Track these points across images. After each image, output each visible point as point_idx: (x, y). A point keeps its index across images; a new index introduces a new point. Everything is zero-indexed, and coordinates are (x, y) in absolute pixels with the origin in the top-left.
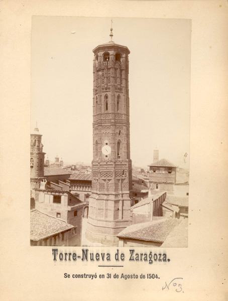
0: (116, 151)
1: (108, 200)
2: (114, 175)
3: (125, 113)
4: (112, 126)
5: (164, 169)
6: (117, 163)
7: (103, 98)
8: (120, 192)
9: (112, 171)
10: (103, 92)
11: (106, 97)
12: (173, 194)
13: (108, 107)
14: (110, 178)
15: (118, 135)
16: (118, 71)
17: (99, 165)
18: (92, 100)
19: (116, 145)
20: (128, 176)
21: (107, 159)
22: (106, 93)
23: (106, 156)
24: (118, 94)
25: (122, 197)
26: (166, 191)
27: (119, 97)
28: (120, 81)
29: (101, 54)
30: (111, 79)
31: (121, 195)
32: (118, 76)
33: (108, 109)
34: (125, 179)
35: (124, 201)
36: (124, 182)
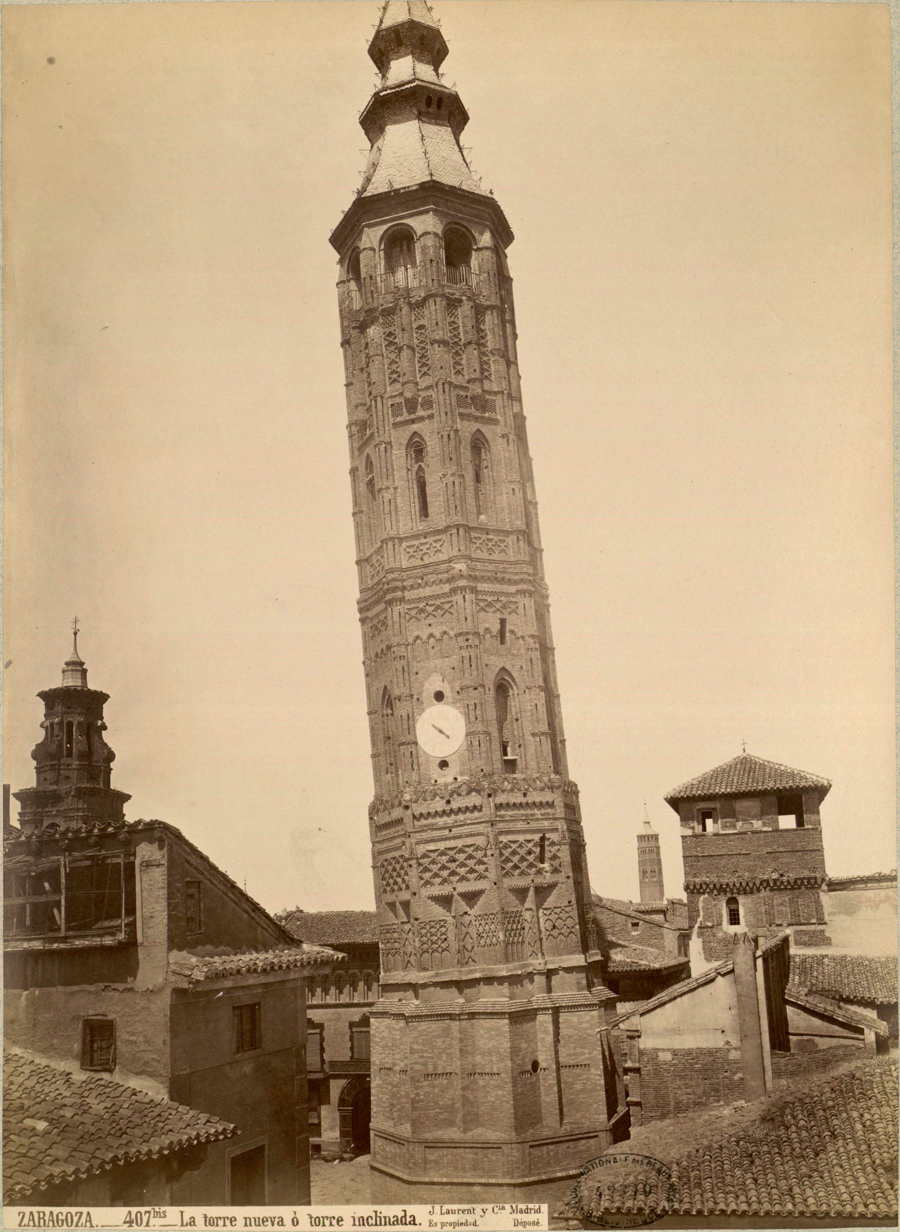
0: (494, 730)
1: (472, 1016)
6: (501, 798)
8: (537, 963)
9: (480, 841)
10: (396, 425)
11: (417, 449)
12: (827, 942)
15: (491, 642)
16: (466, 309)
18: (348, 479)
19: (491, 695)
20: (567, 870)
21: (446, 778)
22: (415, 427)
23: (444, 764)
26: (789, 931)
30: (437, 354)
31: (540, 980)
33: (431, 510)
35: (563, 1017)
36: (550, 901)
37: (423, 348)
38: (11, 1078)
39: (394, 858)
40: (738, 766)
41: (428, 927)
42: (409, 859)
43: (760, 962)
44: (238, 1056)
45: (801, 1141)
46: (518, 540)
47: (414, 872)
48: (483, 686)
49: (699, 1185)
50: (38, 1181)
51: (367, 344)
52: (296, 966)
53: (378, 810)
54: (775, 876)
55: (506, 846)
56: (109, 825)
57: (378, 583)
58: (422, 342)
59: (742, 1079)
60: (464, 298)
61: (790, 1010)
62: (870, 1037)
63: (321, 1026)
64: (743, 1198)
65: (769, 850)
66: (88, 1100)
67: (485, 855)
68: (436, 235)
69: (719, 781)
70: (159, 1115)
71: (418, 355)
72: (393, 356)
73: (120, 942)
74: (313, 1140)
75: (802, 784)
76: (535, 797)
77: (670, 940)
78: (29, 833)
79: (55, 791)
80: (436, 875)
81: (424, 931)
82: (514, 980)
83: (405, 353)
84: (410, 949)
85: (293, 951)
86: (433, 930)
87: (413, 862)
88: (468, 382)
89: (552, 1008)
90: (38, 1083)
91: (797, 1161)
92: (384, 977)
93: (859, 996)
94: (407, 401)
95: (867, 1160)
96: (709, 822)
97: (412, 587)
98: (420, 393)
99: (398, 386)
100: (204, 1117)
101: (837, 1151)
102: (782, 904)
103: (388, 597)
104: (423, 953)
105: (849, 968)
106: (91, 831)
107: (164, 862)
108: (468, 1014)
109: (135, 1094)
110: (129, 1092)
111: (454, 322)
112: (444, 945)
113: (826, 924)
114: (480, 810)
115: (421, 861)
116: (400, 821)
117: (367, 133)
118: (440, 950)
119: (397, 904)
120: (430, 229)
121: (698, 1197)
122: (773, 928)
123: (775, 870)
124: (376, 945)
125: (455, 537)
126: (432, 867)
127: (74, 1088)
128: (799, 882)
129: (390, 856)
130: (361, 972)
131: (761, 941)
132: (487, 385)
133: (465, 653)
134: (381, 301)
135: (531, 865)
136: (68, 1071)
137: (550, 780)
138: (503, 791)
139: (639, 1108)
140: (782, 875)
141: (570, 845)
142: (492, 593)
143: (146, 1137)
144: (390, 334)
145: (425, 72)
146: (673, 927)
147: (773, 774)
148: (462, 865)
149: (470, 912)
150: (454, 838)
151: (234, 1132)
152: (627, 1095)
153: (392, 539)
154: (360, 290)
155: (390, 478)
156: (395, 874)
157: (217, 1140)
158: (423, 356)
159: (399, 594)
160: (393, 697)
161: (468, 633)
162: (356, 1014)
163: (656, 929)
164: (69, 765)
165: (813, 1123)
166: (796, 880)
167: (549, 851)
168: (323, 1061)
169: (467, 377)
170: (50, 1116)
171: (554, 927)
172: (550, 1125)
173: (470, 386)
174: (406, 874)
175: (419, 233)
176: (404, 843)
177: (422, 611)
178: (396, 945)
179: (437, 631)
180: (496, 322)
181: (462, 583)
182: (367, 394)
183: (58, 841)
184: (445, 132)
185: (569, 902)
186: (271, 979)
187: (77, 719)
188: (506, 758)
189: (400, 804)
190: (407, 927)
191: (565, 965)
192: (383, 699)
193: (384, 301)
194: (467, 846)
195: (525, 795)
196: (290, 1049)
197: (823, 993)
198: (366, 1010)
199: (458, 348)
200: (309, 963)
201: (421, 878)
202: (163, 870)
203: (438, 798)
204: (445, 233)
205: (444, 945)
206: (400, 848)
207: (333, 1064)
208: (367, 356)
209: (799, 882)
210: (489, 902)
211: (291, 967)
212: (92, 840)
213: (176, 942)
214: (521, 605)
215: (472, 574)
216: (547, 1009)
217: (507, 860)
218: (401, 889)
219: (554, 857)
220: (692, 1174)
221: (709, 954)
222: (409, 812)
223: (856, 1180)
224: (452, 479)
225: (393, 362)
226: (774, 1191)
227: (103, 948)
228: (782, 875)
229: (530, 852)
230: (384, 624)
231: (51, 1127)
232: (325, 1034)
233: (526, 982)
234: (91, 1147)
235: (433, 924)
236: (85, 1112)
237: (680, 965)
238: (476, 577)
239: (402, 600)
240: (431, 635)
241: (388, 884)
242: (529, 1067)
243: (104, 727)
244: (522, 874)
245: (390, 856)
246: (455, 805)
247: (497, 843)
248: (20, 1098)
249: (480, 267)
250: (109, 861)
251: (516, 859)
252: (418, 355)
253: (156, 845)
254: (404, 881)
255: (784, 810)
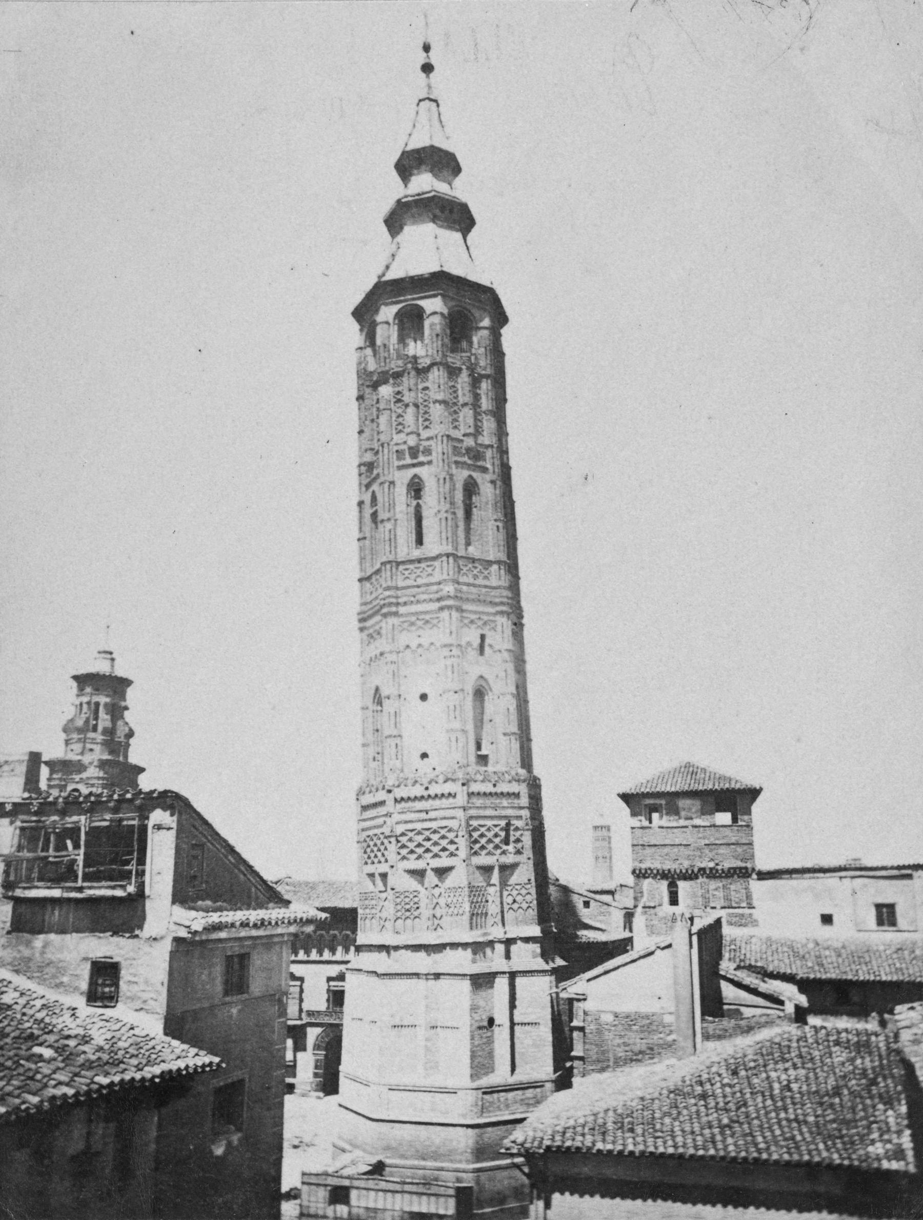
0: (470, 727)
2: (462, 843)
3: (503, 556)
4: (445, 614)
5: (696, 804)
6: (475, 787)
7: (401, 491)
8: (497, 933)
9: (453, 824)
10: (400, 468)
11: (416, 488)
12: (755, 923)
13: (425, 531)
14: (444, 862)
15: (473, 654)
16: (464, 378)
17: (390, 799)
19: (470, 698)
20: (528, 852)
22: (416, 470)
24: (466, 473)
25: (508, 956)
26: (723, 913)
27: (471, 489)
28: (471, 421)
29: (387, 313)
31: (500, 948)
32: (461, 400)
33: (426, 539)
34: (514, 866)
35: (520, 981)
36: (513, 880)
37: (425, 406)
38: (24, 1010)
39: (376, 835)
40: (683, 769)
41: (402, 896)
42: (390, 837)
43: (695, 939)
44: (228, 999)
45: (725, 1096)
46: (500, 569)
47: (393, 847)
48: (462, 690)
49: (632, 1130)
50: (42, 1102)
51: (378, 400)
52: (283, 923)
53: (364, 793)
54: (712, 865)
55: (475, 829)
56: (128, 792)
57: (376, 598)
58: (425, 401)
59: (674, 1040)
60: (464, 367)
61: (724, 984)
62: (790, 1008)
63: (301, 979)
64: (670, 1143)
65: (707, 842)
66: (90, 1032)
67: (457, 836)
68: (442, 314)
69: (665, 780)
70: (154, 1048)
71: (421, 412)
72: (400, 411)
73: (129, 894)
74: (289, 1080)
75: (738, 786)
76: (504, 788)
77: (618, 917)
78: (57, 794)
79: (79, 761)
80: (412, 852)
81: (398, 900)
82: (478, 948)
83: (411, 410)
84: (384, 915)
85: (283, 910)
86: (407, 900)
87: (393, 840)
88: (464, 435)
89: (509, 973)
90: (47, 1015)
91: (720, 1112)
92: (361, 939)
93: (782, 971)
94: (410, 448)
95: (783, 1115)
96: (655, 816)
97: (405, 604)
98: (422, 443)
99: (402, 436)
100: (193, 1051)
101: (756, 1106)
102: (716, 889)
103: (385, 610)
104: (397, 919)
105: (774, 947)
106: (111, 796)
107: (174, 825)
108: (435, 974)
109: (132, 1028)
110: (128, 1026)
111: (454, 386)
112: (416, 913)
113: (754, 908)
114: (455, 796)
115: (400, 839)
116: (382, 803)
117: (389, 230)
118: (412, 917)
119: (377, 875)
120: (438, 310)
121: (630, 1140)
122: (708, 909)
123: (712, 860)
124: (354, 911)
125: (445, 564)
126: (409, 844)
127: (78, 1021)
128: (732, 871)
129: (371, 833)
130: (340, 933)
131: (696, 920)
132: (480, 440)
133: (449, 662)
134: (393, 366)
135: (497, 847)
136: (74, 1006)
137: (517, 774)
138: (475, 781)
139: (581, 1063)
140: (717, 864)
141: (532, 830)
142: (475, 612)
143: (141, 1066)
144: (399, 393)
145: (442, 188)
146: (621, 906)
147: (712, 777)
148: (436, 844)
149: (440, 884)
150: (430, 820)
151: (218, 1065)
152: (571, 1020)
153: (390, 562)
154: (375, 355)
155: (392, 511)
156: (375, 849)
157: (203, 1071)
158: (426, 413)
159: (394, 609)
160: (383, 695)
161: (451, 645)
162: (334, 970)
163: (606, 907)
164: (93, 739)
165: (736, 1081)
166: (730, 869)
167: (513, 836)
168: (301, 1010)
169: (462, 432)
170: (56, 1045)
171: (514, 901)
172: (501, 1075)
173: (465, 438)
174: (386, 849)
175: (428, 312)
176: (385, 822)
177: (412, 624)
178: (374, 911)
179: (425, 641)
180: (490, 388)
181: (450, 602)
182: (376, 440)
183: (81, 803)
184: (458, 236)
185: (529, 880)
186: (261, 933)
187: (103, 700)
188: (479, 753)
189: (383, 789)
190: (384, 895)
191: (523, 935)
192: (375, 697)
193: (395, 365)
194: (442, 828)
195: (495, 785)
196: (274, 995)
197: (750, 968)
198: (342, 967)
199: (456, 408)
200: (295, 921)
201: (399, 853)
202: (173, 833)
203: (418, 785)
204: (450, 314)
205: (416, 913)
206: (380, 826)
207: (310, 1013)
208: (378, 409)
209: (732, 871)
210: (459, 877)
211: (280, 923)
212: (112, 804)
213: (181, 897)
214: (499, 624)
215: (459, 595)
216: (504, 973)
217: (476, 842)
218: (380, 862)
219: (518, 841)
220: (626, 1121)
221: (651, 930)
222: (391, 796)
223: (772, 1131)
224: (445, 515)
225: (399, 416)
226: (699, 1138)
227: (114, 898)
228: (717, 864)
229: (496, 835)
230: (379, 633)
231: (56, 1055)
232: (305, 986)
233: (488, 951)
234: (89, 1074)
235: (407, 894)
236: (87, 1042)
237: (624, 940)
238: (461, 598)
239: (396, 614)
240: (420, 645)
241: (369, 857)
242: (485, 1024)
243: (126, 708)
244: (489, 853)
245: (371, 833)
246: (432, 792)
247: (468, 825)
248: (31, 1028)
249: (479, 343)
250: (125, 823)
251: (483, 841)
252: (421, 412)
253: (168, 813)
254: (383, 855)
255: (720, 809)
